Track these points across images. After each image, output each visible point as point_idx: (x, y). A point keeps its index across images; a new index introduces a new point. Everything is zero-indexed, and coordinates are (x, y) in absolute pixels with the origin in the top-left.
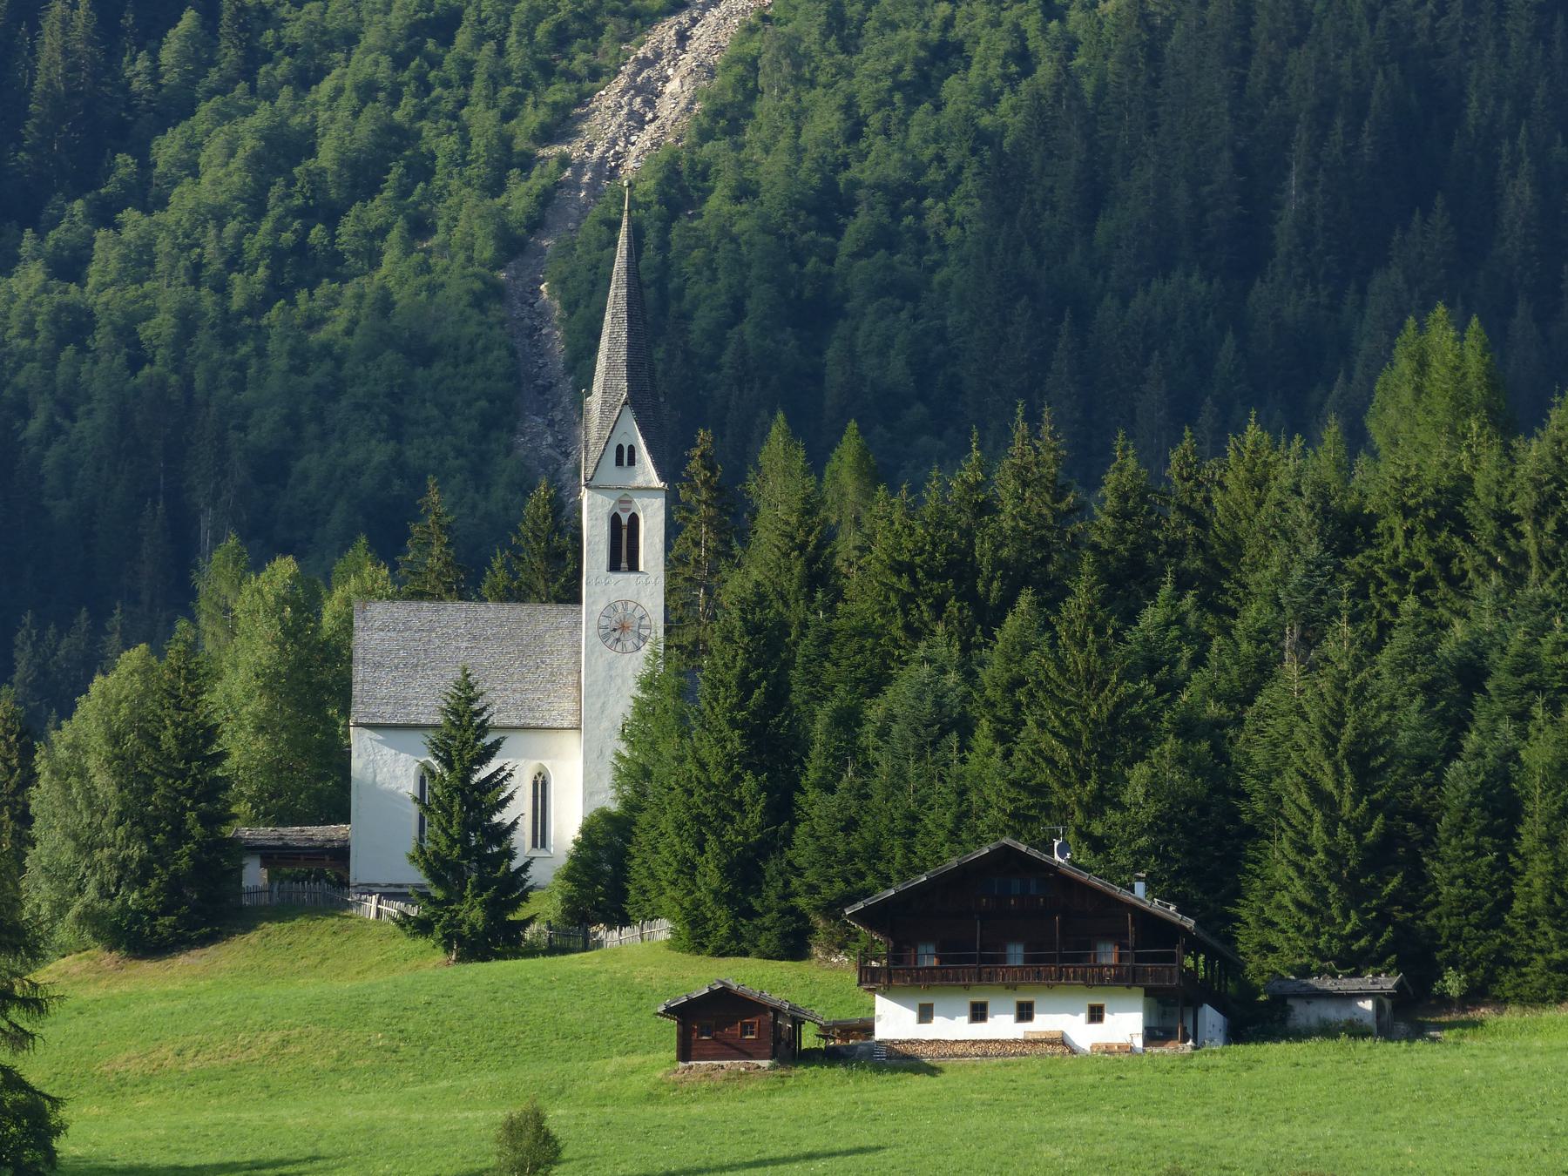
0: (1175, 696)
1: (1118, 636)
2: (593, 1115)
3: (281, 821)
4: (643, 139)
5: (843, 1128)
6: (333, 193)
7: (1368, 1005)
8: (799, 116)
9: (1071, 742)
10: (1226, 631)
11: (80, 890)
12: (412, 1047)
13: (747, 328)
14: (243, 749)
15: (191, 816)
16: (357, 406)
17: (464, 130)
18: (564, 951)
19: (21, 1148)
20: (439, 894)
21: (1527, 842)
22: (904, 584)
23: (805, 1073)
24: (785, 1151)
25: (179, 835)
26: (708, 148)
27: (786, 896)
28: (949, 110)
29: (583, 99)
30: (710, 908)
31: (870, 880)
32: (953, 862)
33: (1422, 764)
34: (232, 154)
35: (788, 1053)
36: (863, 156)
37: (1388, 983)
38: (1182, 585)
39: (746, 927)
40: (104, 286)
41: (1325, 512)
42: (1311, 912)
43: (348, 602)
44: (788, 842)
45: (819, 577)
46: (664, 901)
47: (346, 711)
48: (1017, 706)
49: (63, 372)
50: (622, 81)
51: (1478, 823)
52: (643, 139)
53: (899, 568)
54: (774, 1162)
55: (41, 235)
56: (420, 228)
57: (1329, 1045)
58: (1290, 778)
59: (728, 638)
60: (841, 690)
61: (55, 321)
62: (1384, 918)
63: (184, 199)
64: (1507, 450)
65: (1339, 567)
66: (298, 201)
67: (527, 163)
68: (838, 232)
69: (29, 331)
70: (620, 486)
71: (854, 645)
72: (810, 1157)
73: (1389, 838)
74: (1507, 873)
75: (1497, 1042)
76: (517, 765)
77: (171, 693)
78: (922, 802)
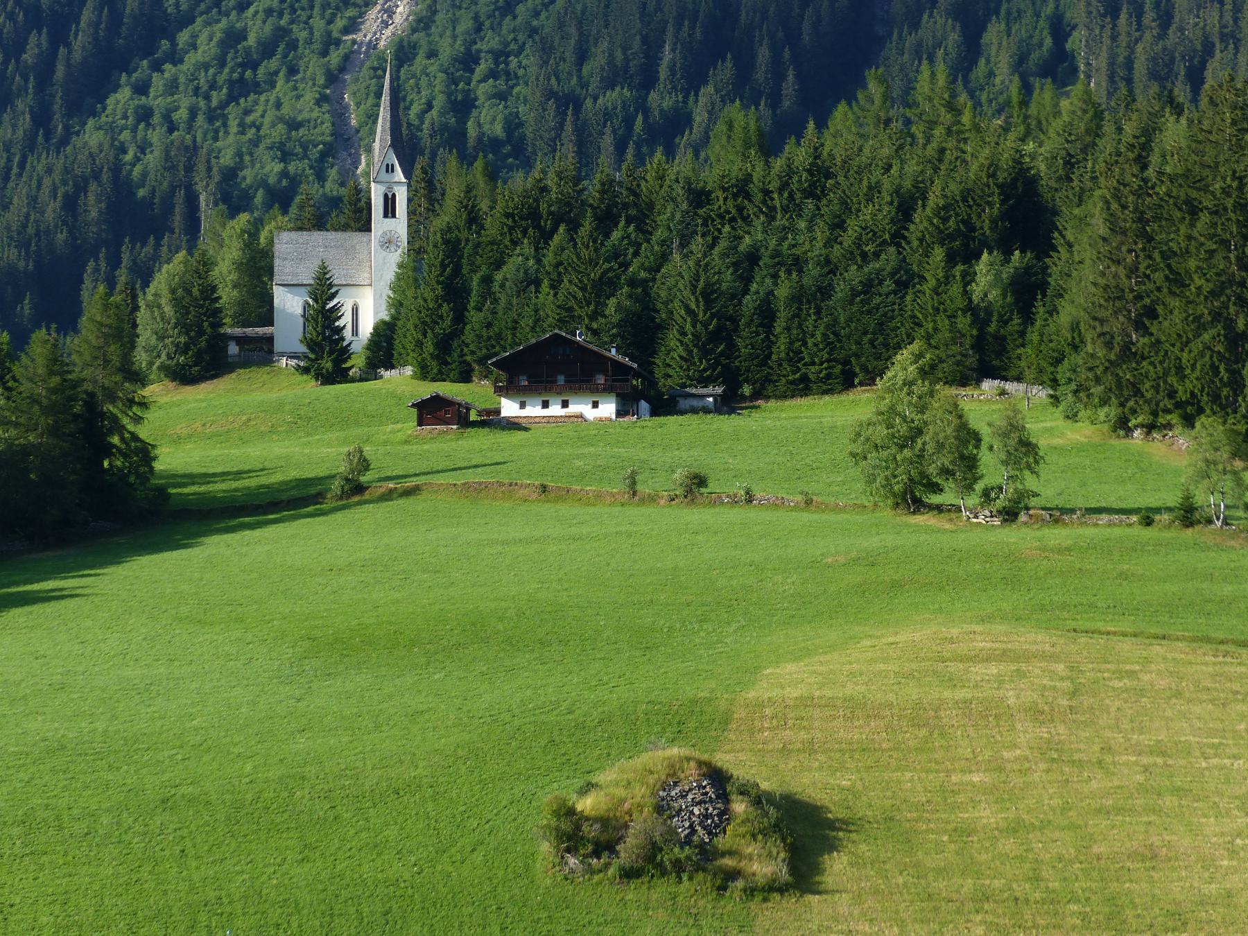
0: (627, 268)
1: (602, 244)
2: (382, 450)
3: (244, 326)
4: (388, 32)
5: (489, 454)
6: (255, 56)
7: (711, 399)
8: (454, 22)
9: (583, 289)
10: (648, 241)
11: (159, 356)
12: (303, 421)
13: (434, 112)
14: (227, 295)
15: (206, 324)
16: (268, 148)
17: (311, 29)
18: (367, 380)
19: (139, 466)
20: (312, 356)
21: (778, 330)
22: (510, 222)
23: (472, 431)
24: (465, 464)
25: (201, 332)
26: (416, 35)
27: (462, 355)
28: (519, 19)
29: (362, 15)
30: (429, 361)
31: (497, 348)
32: (533, 341)
33: (733, 297)
34: (211, 40)
35: (465, 423)
36: (482, 39)
37: (719, 390)
38: (628, 223)
39: (445, 369)
40: (156, 97)
41: (689, 190)
42: (686, 360)
43: (271, 232)
44: (462, 333)
45: (474, 219)
46: (409, 358)
47: (271, 279)
48: (560, 274)
49: (140, 134)
50: (379, 7)
51: (757, 322)
52: (388, 32)
53: (507, 216)
54: (460, 469)
55: (129, 74)
56: (292, 71)
57: (695, 416)
58: (677, 304)
59: (435, 246)
60: (484, 268)
61: (136, 112)
62: (717, 363)
63: (191, 59)
64: (767, 163)
65: (696, 213)
66: (240, 60)
67: (338, 43)
68: (472, 71)
69: (125, 117)
70: (385, 180)
71: (489, 248)
72: (476, 466)
73: (719, 328)
74: (769, 343)
75: (767, 414)
76: (345, 301)
77: (197, 272)
78: (519, 315)
